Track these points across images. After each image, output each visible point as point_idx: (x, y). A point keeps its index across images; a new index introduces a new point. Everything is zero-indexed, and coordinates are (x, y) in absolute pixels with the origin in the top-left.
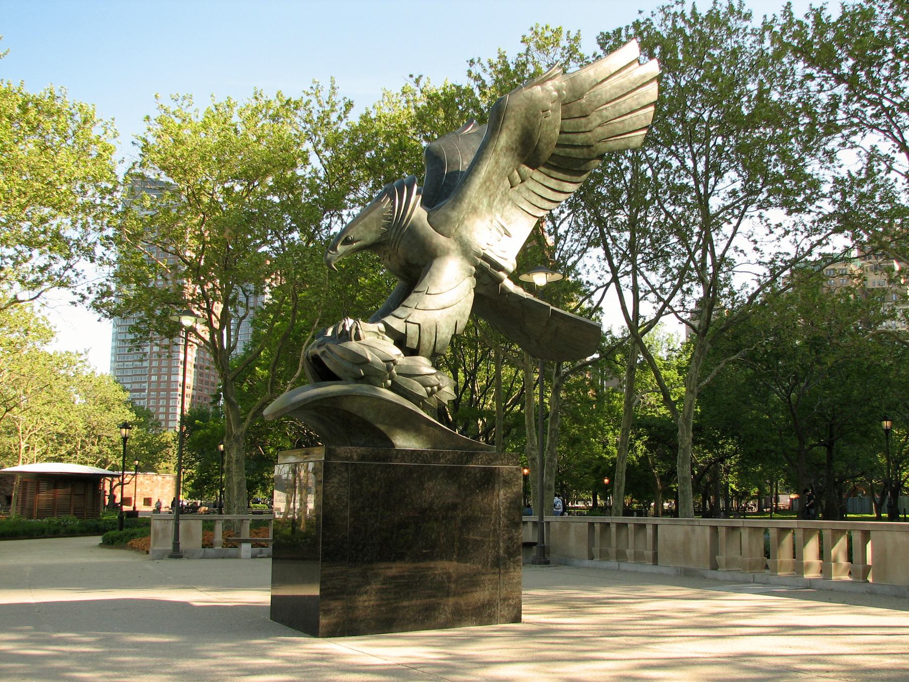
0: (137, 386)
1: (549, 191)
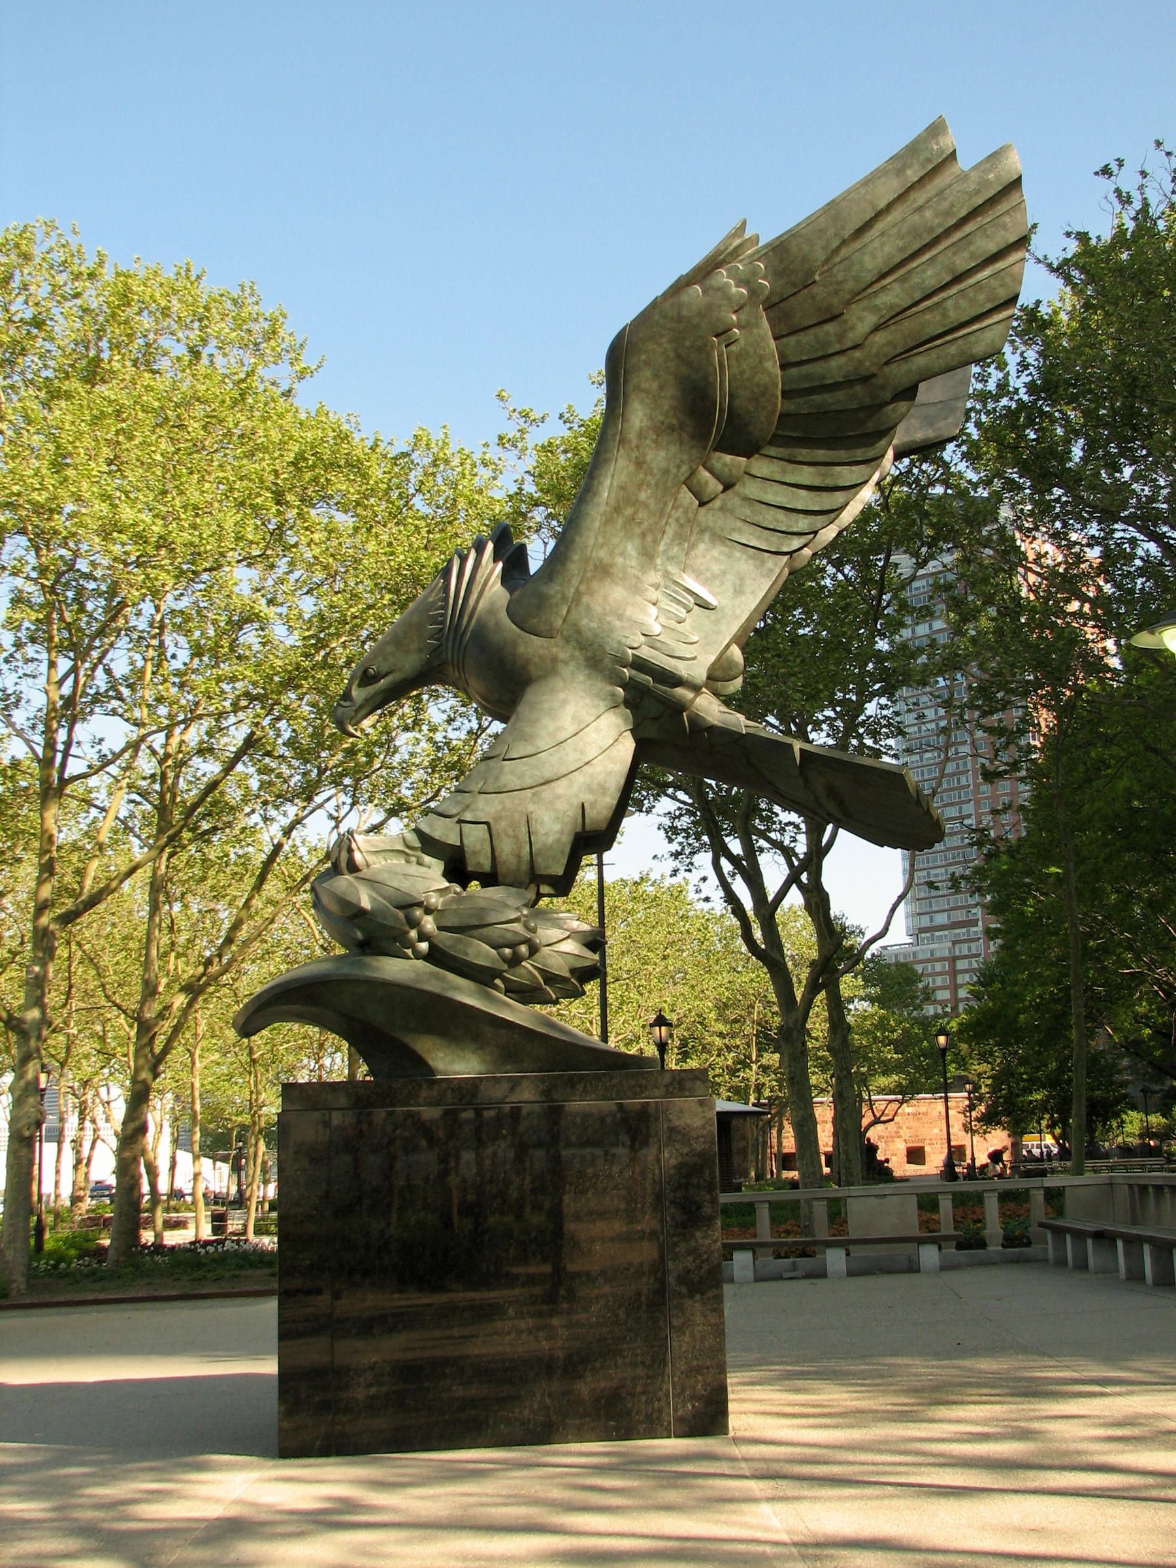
0: (960, 916)
1: (803, 493)
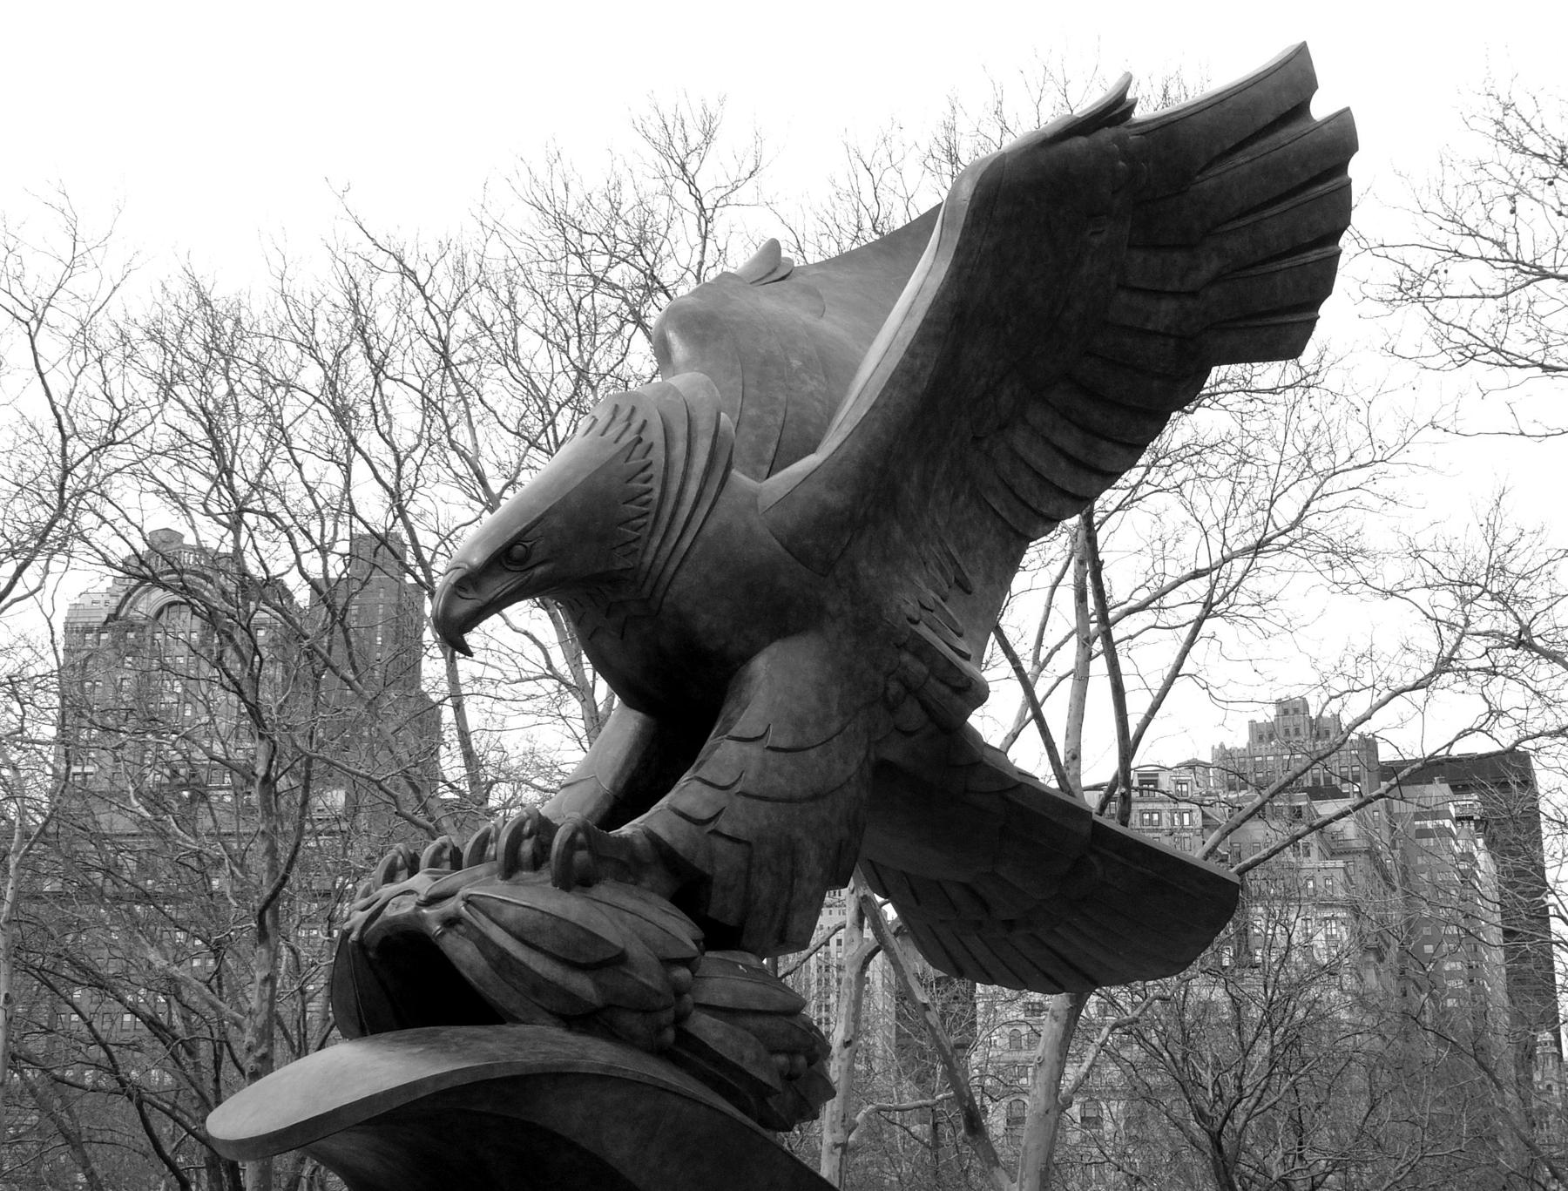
1: (1063, 464)
